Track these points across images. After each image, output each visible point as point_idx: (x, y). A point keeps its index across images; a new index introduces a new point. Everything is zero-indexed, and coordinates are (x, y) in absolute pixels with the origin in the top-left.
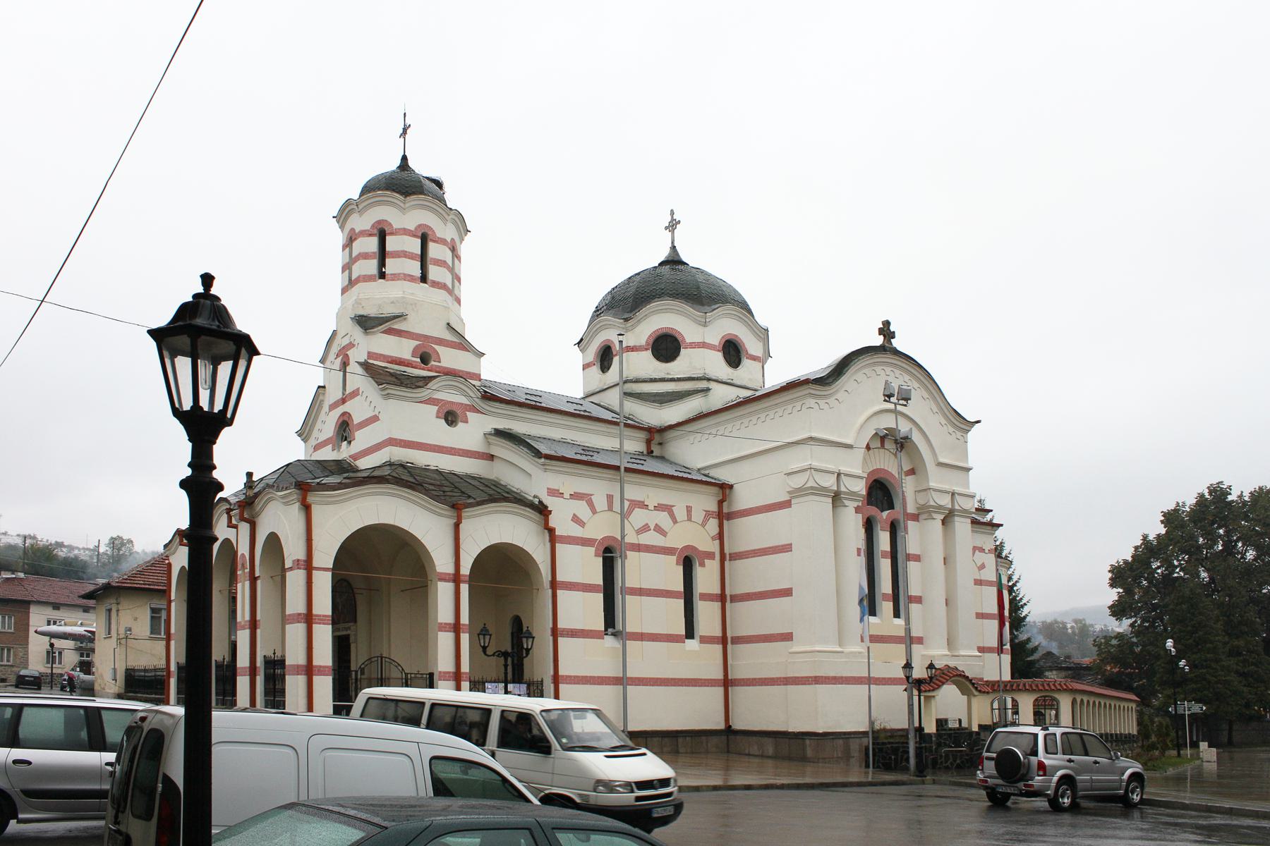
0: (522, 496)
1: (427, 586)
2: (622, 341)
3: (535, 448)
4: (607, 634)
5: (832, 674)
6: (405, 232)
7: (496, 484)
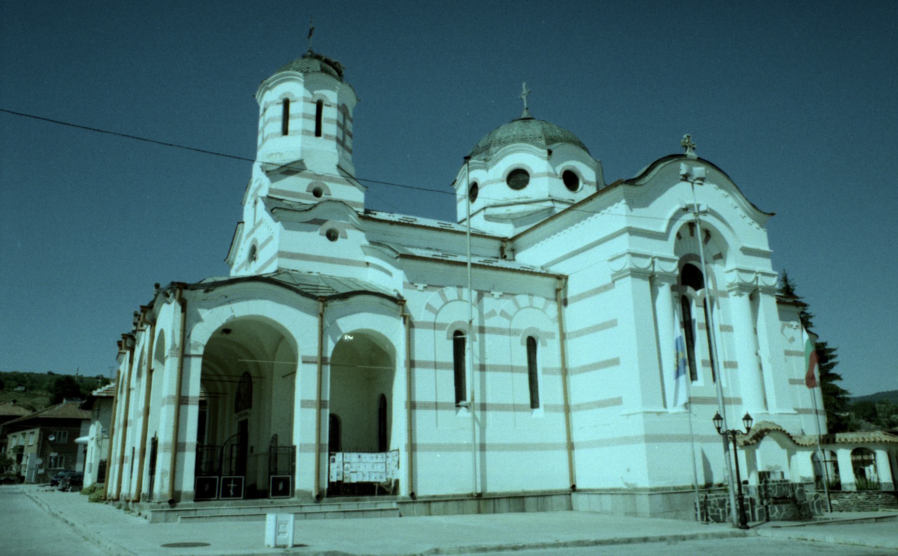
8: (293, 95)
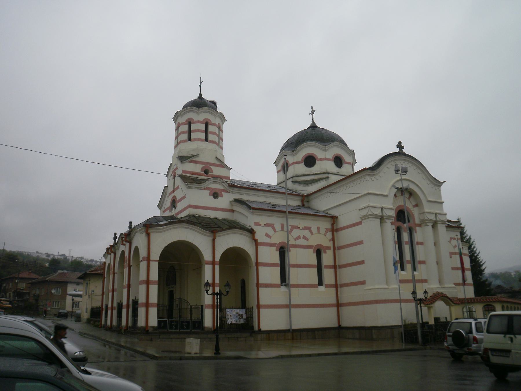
0: (245, 226)
1: (201, 267)
2: (286, 158)
3: (249, 206)
4: (282, 285)
5: (384, 299)
6: (199, 122)
7: (234, 222)
8: (193, 119)
